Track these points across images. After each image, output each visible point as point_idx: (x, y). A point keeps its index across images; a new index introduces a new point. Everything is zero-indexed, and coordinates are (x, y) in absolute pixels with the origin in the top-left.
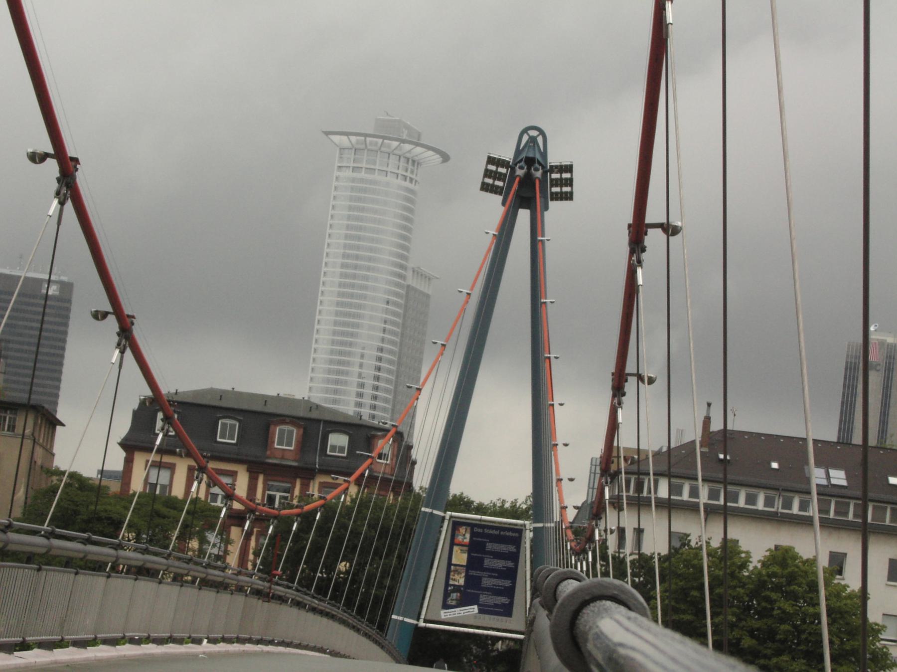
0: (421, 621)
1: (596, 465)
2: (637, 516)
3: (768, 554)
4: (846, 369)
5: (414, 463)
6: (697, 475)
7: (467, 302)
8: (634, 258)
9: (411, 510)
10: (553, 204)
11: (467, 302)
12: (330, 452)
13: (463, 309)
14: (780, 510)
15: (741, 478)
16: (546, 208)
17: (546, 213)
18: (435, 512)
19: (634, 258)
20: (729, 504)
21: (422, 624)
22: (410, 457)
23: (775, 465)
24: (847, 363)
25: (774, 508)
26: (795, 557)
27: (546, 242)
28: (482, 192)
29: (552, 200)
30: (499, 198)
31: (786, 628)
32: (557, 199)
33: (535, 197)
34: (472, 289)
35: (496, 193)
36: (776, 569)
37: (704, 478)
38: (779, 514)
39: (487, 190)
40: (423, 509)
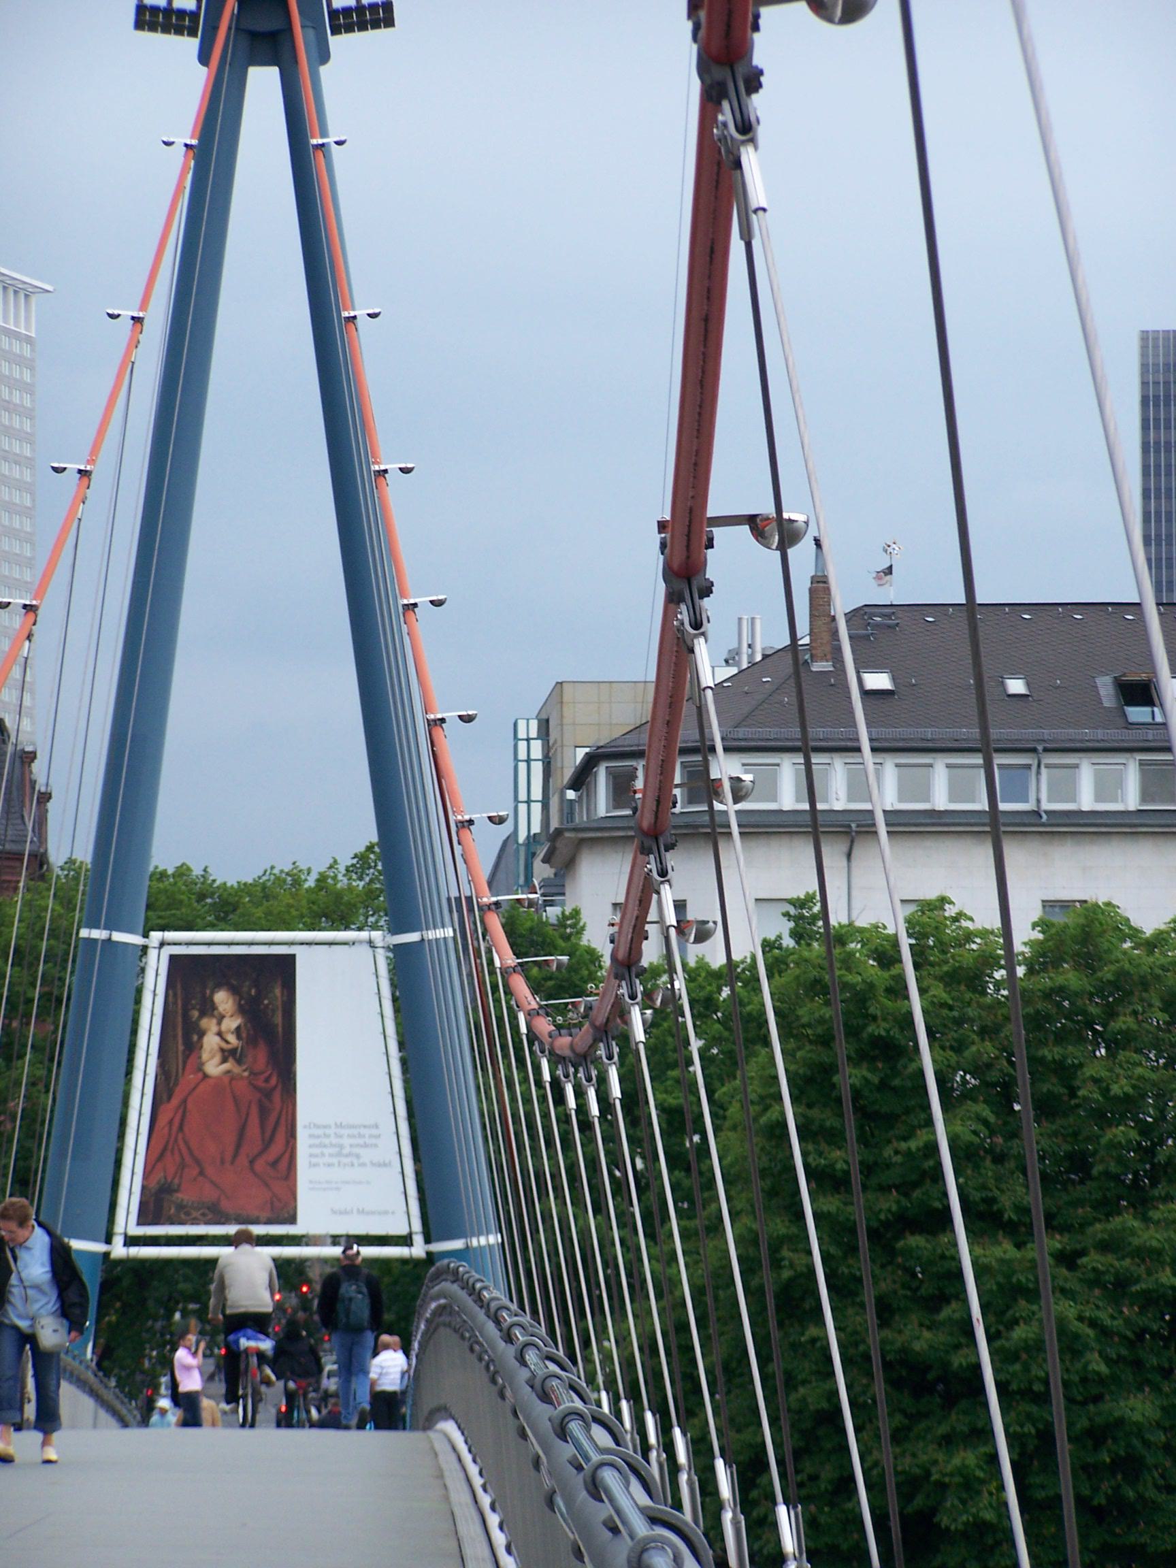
0: (118, 1241)
1: (528, 740)
2: (846, 875)
3: (236, 885)
4: (1145, 401)
5: (45, 797)
6: (858, 740)
7: (134, 343)
8: (726, 115)
9: (53, 934)
10: (338, 43)
11: (134, 343)
12: (1050, 800)
13: (127, 366)
14: (1046, 806)
15: (929, 733)
16: (324, 57)
17: (323, 70)
18: (118, 937)
19: (726, 115)
20: (1003, 806)
21: (119, 1250)
22: (33, 783)
23: (1016, 686)
24: (1144, 384)
25: (1027, 801)
26: (1124, 930)
27: (334, 147)
28: (146, 36)
29: (336, 31)
30: (191, 45)
31: (984, 1114)
32: (349, 29)
33: (290, 29)
34: (144, 305)
35: (179, 31)
36: (1069, 976)
37: (876, 744)
38: (1045, 817)
39: (153, 27)
40: (84, 933)
